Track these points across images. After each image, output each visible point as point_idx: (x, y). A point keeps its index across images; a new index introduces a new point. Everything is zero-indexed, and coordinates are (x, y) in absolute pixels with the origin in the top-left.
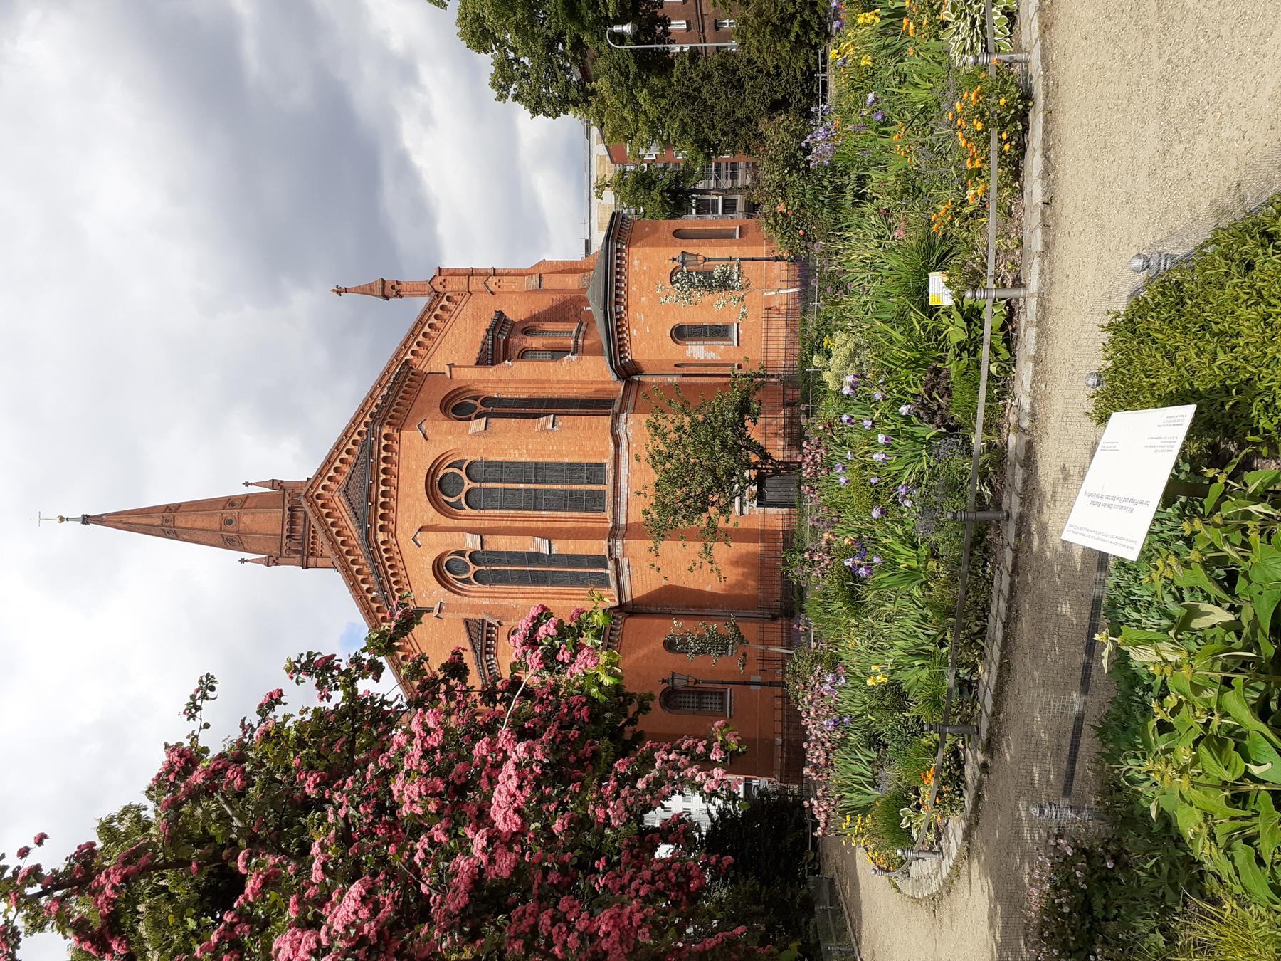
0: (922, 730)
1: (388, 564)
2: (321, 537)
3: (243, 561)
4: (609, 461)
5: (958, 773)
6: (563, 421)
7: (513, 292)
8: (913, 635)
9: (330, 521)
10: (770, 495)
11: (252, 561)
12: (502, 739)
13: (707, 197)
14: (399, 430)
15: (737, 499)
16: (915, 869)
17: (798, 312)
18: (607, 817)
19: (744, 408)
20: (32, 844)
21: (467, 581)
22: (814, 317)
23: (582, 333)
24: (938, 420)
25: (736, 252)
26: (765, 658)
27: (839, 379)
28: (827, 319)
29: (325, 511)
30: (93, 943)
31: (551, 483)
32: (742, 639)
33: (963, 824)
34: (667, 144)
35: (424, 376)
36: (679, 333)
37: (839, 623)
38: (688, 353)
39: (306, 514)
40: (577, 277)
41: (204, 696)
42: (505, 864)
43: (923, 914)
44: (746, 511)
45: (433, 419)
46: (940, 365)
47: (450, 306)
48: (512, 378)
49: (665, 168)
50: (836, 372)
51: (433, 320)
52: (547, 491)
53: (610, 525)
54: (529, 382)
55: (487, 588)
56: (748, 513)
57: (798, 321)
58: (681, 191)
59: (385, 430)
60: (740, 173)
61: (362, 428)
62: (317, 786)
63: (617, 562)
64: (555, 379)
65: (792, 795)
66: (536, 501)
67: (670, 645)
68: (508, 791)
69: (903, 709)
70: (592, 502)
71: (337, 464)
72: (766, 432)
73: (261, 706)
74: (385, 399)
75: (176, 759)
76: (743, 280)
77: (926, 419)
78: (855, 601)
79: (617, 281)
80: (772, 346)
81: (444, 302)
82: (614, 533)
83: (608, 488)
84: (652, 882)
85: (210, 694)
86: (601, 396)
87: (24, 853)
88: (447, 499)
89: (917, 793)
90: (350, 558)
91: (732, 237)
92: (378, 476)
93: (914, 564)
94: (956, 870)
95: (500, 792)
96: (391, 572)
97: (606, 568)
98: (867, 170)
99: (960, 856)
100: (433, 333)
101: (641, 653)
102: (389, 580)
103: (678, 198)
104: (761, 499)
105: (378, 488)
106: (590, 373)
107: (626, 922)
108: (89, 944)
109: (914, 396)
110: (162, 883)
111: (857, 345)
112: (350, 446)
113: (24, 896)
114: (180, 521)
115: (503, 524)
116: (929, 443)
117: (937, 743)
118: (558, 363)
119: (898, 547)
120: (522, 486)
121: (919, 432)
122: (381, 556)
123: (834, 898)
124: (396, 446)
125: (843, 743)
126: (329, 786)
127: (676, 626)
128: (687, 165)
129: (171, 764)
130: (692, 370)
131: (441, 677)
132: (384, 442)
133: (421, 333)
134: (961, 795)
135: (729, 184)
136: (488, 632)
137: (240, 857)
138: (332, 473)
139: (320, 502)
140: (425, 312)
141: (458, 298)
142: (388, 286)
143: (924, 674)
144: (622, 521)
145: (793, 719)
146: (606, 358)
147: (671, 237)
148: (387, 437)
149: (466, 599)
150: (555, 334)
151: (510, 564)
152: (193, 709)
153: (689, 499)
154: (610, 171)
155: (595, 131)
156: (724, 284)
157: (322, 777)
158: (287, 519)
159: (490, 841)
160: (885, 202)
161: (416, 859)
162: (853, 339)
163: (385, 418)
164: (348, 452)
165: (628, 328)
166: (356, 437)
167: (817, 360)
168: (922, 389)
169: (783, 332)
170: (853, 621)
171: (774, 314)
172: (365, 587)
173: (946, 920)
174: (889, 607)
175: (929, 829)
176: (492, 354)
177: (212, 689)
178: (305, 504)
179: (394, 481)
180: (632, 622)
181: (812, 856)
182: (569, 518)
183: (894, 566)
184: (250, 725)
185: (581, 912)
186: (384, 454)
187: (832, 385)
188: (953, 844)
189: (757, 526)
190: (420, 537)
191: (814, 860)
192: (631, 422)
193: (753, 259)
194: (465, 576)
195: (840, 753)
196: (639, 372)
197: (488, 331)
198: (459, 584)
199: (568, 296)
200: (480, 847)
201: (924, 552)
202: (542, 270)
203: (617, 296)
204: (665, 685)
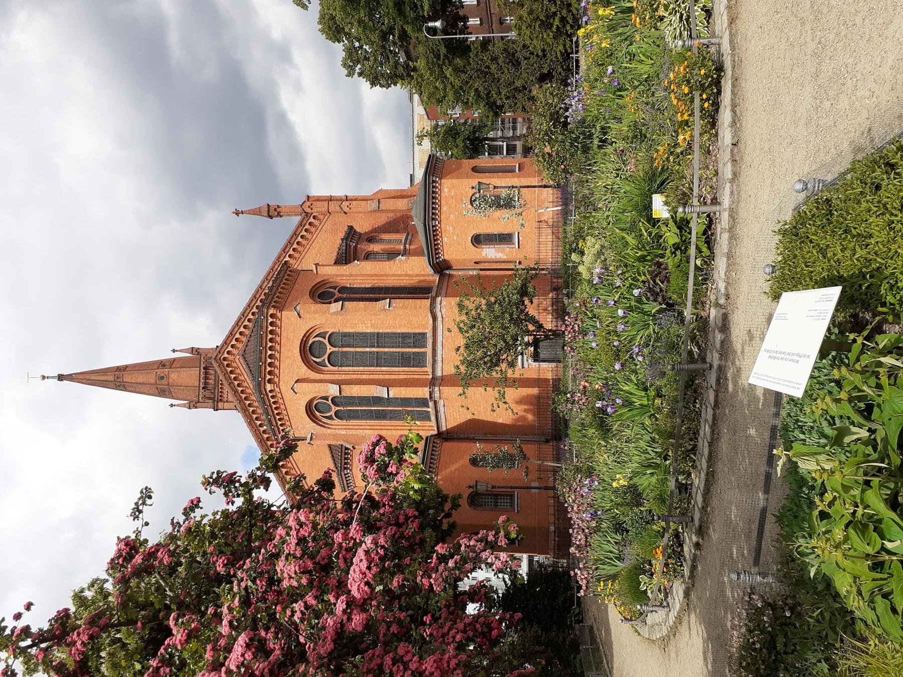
0: (653, 520)
1: (274, 406)
2: (226, 388)
3: (172, 405)
4: (429, 331)
6: (396, 303)
9: (233, 376)
11: (178, 405)
12: (352, 530)
13: (496, 143)
14: (281, 311)
15: (520, 357)
16: (650, 619)
17: (561, 224)
18: (431, 585)
19: (523, 292)
20: (23, 610)
21: (330, 418)
24: (660, 299)
25: (516, 182)
26: (541, 469)
28: (581, 228)
29: (229, 369)
32: (524, 457)
34: (466, 105)
35: (298, 272)
36: (478, 240)
38: (484, 254)
39: (216, 372)
40: (405, 201)
41: (144, 503)
42: (357, 620)
43: (656, 651)
44: (526, 366)
45: (305, 303)
46: (661, 260)
47: (316, 222)
48: (360, 273)
50: (588, 266)
51: (304, 233)
52: (385, 353)
53: (431, 377)
54: (372, 276)
55: (344, 422)
56: (527, 366)
57: (561, 230)
59: (271, 311)
60: (519, 125)
61: (254, 310)
62: (225, 565)
66: (378, 360)
67: (474, 462)
68: (360, 570)
69: (639, 504)
70: (418, 361)
71: (238, 336)
72: (540, 310)
73: (185, 509)
74: (271, 289)
75: (123, 547)
77: (651, 298)
78: (604, 428)
80: (543, 248)
82: (434, 382)
83: (429, 350)
84: (464, 631)
85: (148, 501)
86: (421, 285)
87: (18, 617)
88: (315, 359)
89: (651, 565)
90: (247, 402)
91: (513, 171)
92: (266, 344)
93: (645, 403)
94: (679, 619)
95: (354, 571)
96: (276, 412)
97: (428, 407)
99: (682, 609)
100: (304, 242)
101: (453, 467)
102: (275, 418)
103: (475, 144)
104: (536, 357)
105: (266, 352)
106: (414, 268)
107: (446, 665)
111: (603, 247)
112: (246, 323)
114: (127, 378)
115: (355, 377)
116: (654, 315)
117: (664, 529)
118: (392, 262)
120: (368, 349)
121: (647, 308)
122: (269, 401)
124: (278, 322)
125: (597, 529)
126: (233, 565)
127: (478, 447)
130: (487, 266)
133: (296, 242)
134: (681, 566)
136: (346, 454)
137: (171, 618)
138: (234, 342)
139: (226, 363)
140: (298, 227)
141: (321, 217)
142: (272, 209)
143: (654, 479)
144: (439, 374)
145: (561, 511)
146: (426, 258)
148: (272, 316)
149: (329, 431)
150: (390, 241)
151: (360, 405)
152: (137, 512)
153: (486, 359)
154: (428, 125)
155: (416, 97)
156: (508, 204)
157: (228, 559)
158: (202, 376)
160: (621, 145)
162: (599, 242)
163: (270, 303)
164: (245, 327)
165: (441, 237)
166: (250, 316)
167: (574, 257)
169: (550, 238)
170: (603, 443)
171: (544, 225)
172: (258, 423)
173: (673, 655)
175: (660, 590)
176: (345, 257)
177: (150, 497)
179: (278, 347)
180: (447, 445)
181: (578, 610)
182: (400, 372)
184: (178, 523)
185: (413, 656)
186: (270, 328)
187: (585, 275)
190: (296, 387)
191: (579, 613)
192: (444, 303)
193: (528, 187)
194: (328, 414)
196: (449, 267)
197: (342, 240)
198: (325, 420)
200: (341, 609)
201: (652, 393)
202: (379, 196)
203: (433, 214)
204: (471, 490)
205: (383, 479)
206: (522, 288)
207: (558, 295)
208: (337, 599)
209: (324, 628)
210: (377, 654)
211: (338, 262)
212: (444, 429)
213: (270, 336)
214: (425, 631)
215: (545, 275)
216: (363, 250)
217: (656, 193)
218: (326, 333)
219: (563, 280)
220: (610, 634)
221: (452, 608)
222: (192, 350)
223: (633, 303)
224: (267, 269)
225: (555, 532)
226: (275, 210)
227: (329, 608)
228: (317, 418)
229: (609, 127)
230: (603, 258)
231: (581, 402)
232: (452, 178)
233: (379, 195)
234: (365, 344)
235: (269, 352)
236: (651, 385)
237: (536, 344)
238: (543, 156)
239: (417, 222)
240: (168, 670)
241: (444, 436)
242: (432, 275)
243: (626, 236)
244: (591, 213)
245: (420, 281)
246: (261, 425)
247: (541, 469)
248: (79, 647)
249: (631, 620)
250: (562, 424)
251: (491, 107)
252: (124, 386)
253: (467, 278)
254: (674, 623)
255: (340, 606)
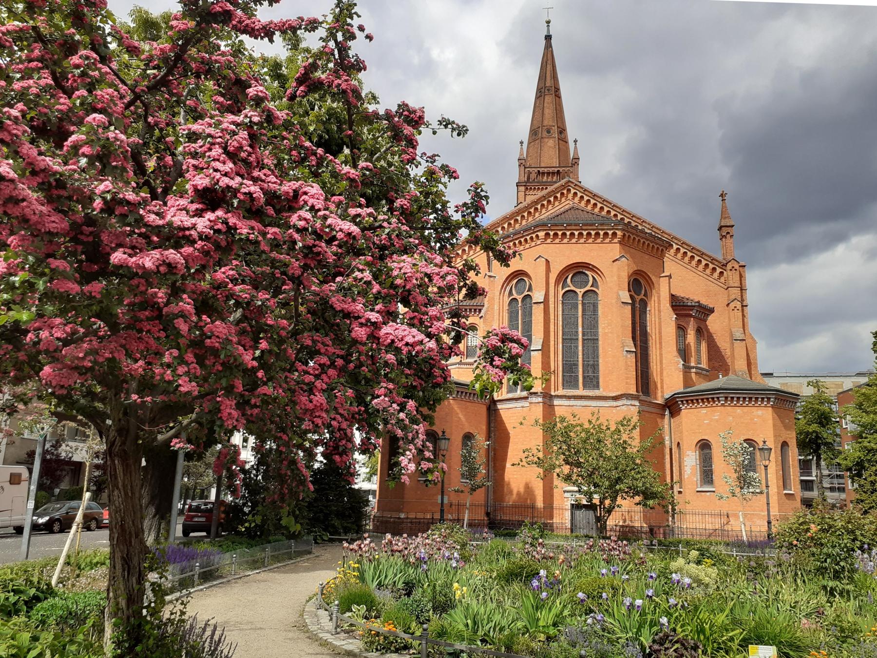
0: (423, 623)
1: (522, 240)
3: (522, 143)
5: (392, 648)
6: (632, 358)
7: (730, 320)
8: (489, 620)
9: (552, 199)
10: (580, 514)
11: (522, 149)
13: (814, 467)
14: (620, 242)
15: (576, 489)
16: (323, 613)
17: (726, 539)
18: (378, 396)
19: (648, 495)
20: (366, 32)
21: (510, 293)
22: (724, 552)
23: (700, 372)
24: (656, 647)
25: (773, 490)
26: (460, 507)
27: (679, 570)
28: (724, 562)
30: (303, 75)
31: (583, 350)
32: (473, 490)
33: (357, 651)
34: (858, 437)
36: (704, 446)
37: (491, 562)
38: (689, 453)
39: (555, 182)
41: (453, 129)
42: (360, 332)
43: (293, 618)
44: (567, 495)
46: (700, 651)
47: (716, 275)
48: (662, 321)
49: (837, 435)
50: (684, 568)
51: (704, 262)
52: (577, 347)
53: (553, 393)
54: (660, 333)
55: (506, 307)
56: (566, 496)
58: (818, 447)
59: (619, 233)
60: (836, 494)
61: (620, 216)
62: (402, 206)
63: (526, 398)
64: (663, 352)
65: (366, 524)
66: (569, 340)
67: (468, 437)
69: (435, 609)
70: (570, 381)
71: (593, 201)
72: (627, 511)
73: (447, 166)
74: (642, 231)
75: (418, 115)
76: (750, 496)
77: (657, 637)
78: (511, 576)
79: (745, 398)
80: (698, 518)
81: (719, 270)
82: (548, 397)
83: (581, 392)
84: (340, 429)
85: (455, 133)
86: (652, 386)
87: (361, 28)
88: (570, 277)
89: (376, 617)
91: (785, 487)
92: (585, 230)
93: (541, 623)
94: (324, 644)
96: (517, 242)
97: (521, 391)
98: (855, 598)
99: (334, 648)
100: (694, 263)
102: (511, 241)
103: (812, 445)
104: (576, 507)
105: (577, 230)
106: (669, 379)
107: (317, 414)
108: (303, 72)
109: (674, 630)
110: (316, 107)
111: (707, 586)
112: (606, 209)
113: (337, 32)
114: (549, 99)
115: (552, 317)
116: (637, 639)
117: (413, 634)
118: (676, 353)
119: (554, 611)
120: (580, 329)
121: (645, 631)
123: (300, 554)
124: (607, 240)
125: (407, 563)
126: (401, 214)
127: (481, 442)
128: (840, 453)
129: (415, 112)
131: (468, 282)
132: (610, 232)
134: (377, 650)
135: (826, 485)
136: (475, 310)
137: (369, 164)
138: (586, 198)
140: (710, 257)
141: (722, 279)
142: (729, 230)
143: (461, 627)
144: (556, 402)
145: (418, 527)
146: (682, 390)
147: (782, 440)
148: (614, 234)
150: (698, 351)
151: (523, 323)
152: (446, 123)
153: (571, 449)
154: (831, 393)
155: (864, 380)
156: (744, 482)
157: (407, 209)
158: (551, 170)
159: (375, 324)
160: (830, 612)
161: (357, 273)
162: (712, 582)
163: (628, 232)
164: (602, 208)
166: (613, 213)
167: (694, 554)
168: (680, 636)
169: (710, 526)
170: (495, 574)
171: (724, 520)
172: (506, 226)
173: (291, 635)
174: (508, 603)
175: (352, 625)
176: (679, 305)
177: (459, 135)
178: (563, 182)
180: (483, 410)
182: (557, 362)
183: (538, 608)
184: (435, 161)
187: (674, 565)
188: (343, 643)
189: (556, 504)
192: (632, 408)
193: (768, 504)
194: (514, 292)
195: (400, 561)
196: (673, 415)
197: (698, 302)
198: (508, 289)
199: (729, 361)
201: (552, 631)
202: (749, 341)
203: (732, 398)
205: (487, 352)
206: (652, 493)
207: (645, 533)
208: (378, 312)
209: (354, 301)
210: (329, 348)
211: (673, 297)
212: (499, 407)
213: (593, 233)
214: (339, 391)
215: (668, 520)
216: (688, 323)
217: (779, 650)
218: (597, 288)
219: (661, 539)
220: (305, 571)
221: (357, 416)
222: (576, 159)
223: (649, 617)
224: (663, 228)
225: (399, 518)
226: (728, 233)
227: (370, 305)
228: (510, 281)
229: (849, 600)
230: (694, 585)
231: (535, 553)
232: (773, 419)
233: (750, 340)
234: (586, 326)
235: (576, 233)
236: (559, 630)
237: (591, 507)
238: (804, 523)
239: (721, 381)
240: (314, 163)
241: (492, 408)
242: (662, 396)
243: (725, 614)
244: (744, 573)
245: (655, 383)
246: (503, 228)
247: (460, 507)
248: (336, 82)
249: (322, 594)
250: (506, 531)
251: (858, 464)
252: (541, 96)
253: (661, 434)
254: (321, 639)
255: (374, 317)
